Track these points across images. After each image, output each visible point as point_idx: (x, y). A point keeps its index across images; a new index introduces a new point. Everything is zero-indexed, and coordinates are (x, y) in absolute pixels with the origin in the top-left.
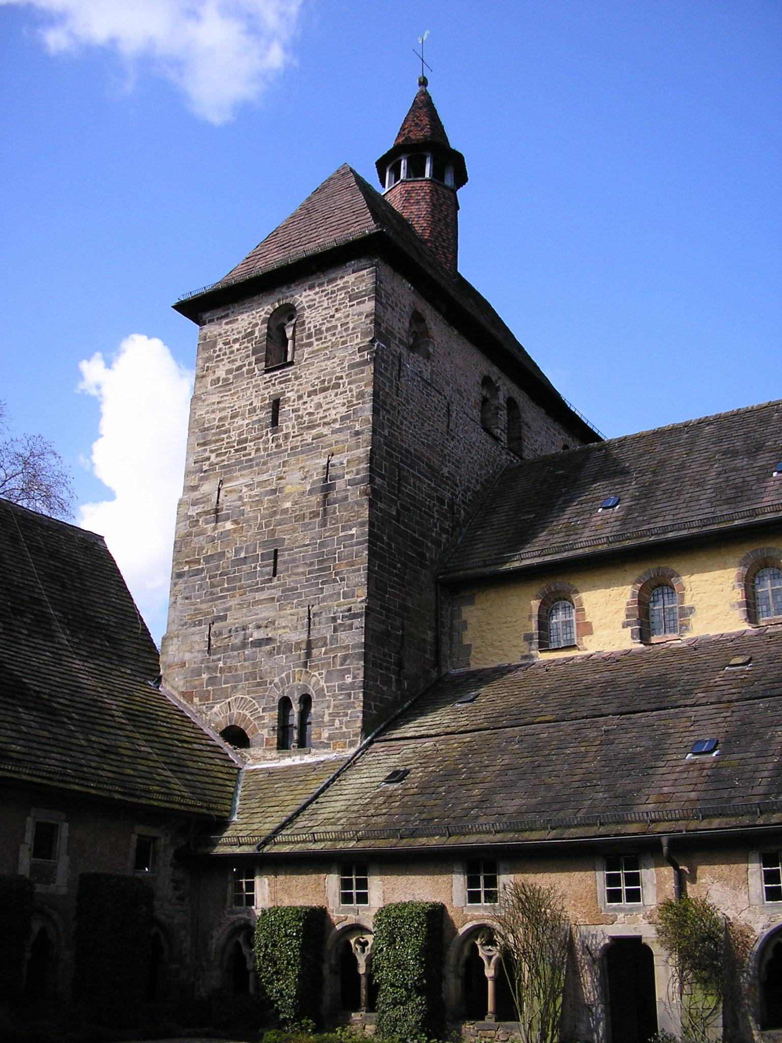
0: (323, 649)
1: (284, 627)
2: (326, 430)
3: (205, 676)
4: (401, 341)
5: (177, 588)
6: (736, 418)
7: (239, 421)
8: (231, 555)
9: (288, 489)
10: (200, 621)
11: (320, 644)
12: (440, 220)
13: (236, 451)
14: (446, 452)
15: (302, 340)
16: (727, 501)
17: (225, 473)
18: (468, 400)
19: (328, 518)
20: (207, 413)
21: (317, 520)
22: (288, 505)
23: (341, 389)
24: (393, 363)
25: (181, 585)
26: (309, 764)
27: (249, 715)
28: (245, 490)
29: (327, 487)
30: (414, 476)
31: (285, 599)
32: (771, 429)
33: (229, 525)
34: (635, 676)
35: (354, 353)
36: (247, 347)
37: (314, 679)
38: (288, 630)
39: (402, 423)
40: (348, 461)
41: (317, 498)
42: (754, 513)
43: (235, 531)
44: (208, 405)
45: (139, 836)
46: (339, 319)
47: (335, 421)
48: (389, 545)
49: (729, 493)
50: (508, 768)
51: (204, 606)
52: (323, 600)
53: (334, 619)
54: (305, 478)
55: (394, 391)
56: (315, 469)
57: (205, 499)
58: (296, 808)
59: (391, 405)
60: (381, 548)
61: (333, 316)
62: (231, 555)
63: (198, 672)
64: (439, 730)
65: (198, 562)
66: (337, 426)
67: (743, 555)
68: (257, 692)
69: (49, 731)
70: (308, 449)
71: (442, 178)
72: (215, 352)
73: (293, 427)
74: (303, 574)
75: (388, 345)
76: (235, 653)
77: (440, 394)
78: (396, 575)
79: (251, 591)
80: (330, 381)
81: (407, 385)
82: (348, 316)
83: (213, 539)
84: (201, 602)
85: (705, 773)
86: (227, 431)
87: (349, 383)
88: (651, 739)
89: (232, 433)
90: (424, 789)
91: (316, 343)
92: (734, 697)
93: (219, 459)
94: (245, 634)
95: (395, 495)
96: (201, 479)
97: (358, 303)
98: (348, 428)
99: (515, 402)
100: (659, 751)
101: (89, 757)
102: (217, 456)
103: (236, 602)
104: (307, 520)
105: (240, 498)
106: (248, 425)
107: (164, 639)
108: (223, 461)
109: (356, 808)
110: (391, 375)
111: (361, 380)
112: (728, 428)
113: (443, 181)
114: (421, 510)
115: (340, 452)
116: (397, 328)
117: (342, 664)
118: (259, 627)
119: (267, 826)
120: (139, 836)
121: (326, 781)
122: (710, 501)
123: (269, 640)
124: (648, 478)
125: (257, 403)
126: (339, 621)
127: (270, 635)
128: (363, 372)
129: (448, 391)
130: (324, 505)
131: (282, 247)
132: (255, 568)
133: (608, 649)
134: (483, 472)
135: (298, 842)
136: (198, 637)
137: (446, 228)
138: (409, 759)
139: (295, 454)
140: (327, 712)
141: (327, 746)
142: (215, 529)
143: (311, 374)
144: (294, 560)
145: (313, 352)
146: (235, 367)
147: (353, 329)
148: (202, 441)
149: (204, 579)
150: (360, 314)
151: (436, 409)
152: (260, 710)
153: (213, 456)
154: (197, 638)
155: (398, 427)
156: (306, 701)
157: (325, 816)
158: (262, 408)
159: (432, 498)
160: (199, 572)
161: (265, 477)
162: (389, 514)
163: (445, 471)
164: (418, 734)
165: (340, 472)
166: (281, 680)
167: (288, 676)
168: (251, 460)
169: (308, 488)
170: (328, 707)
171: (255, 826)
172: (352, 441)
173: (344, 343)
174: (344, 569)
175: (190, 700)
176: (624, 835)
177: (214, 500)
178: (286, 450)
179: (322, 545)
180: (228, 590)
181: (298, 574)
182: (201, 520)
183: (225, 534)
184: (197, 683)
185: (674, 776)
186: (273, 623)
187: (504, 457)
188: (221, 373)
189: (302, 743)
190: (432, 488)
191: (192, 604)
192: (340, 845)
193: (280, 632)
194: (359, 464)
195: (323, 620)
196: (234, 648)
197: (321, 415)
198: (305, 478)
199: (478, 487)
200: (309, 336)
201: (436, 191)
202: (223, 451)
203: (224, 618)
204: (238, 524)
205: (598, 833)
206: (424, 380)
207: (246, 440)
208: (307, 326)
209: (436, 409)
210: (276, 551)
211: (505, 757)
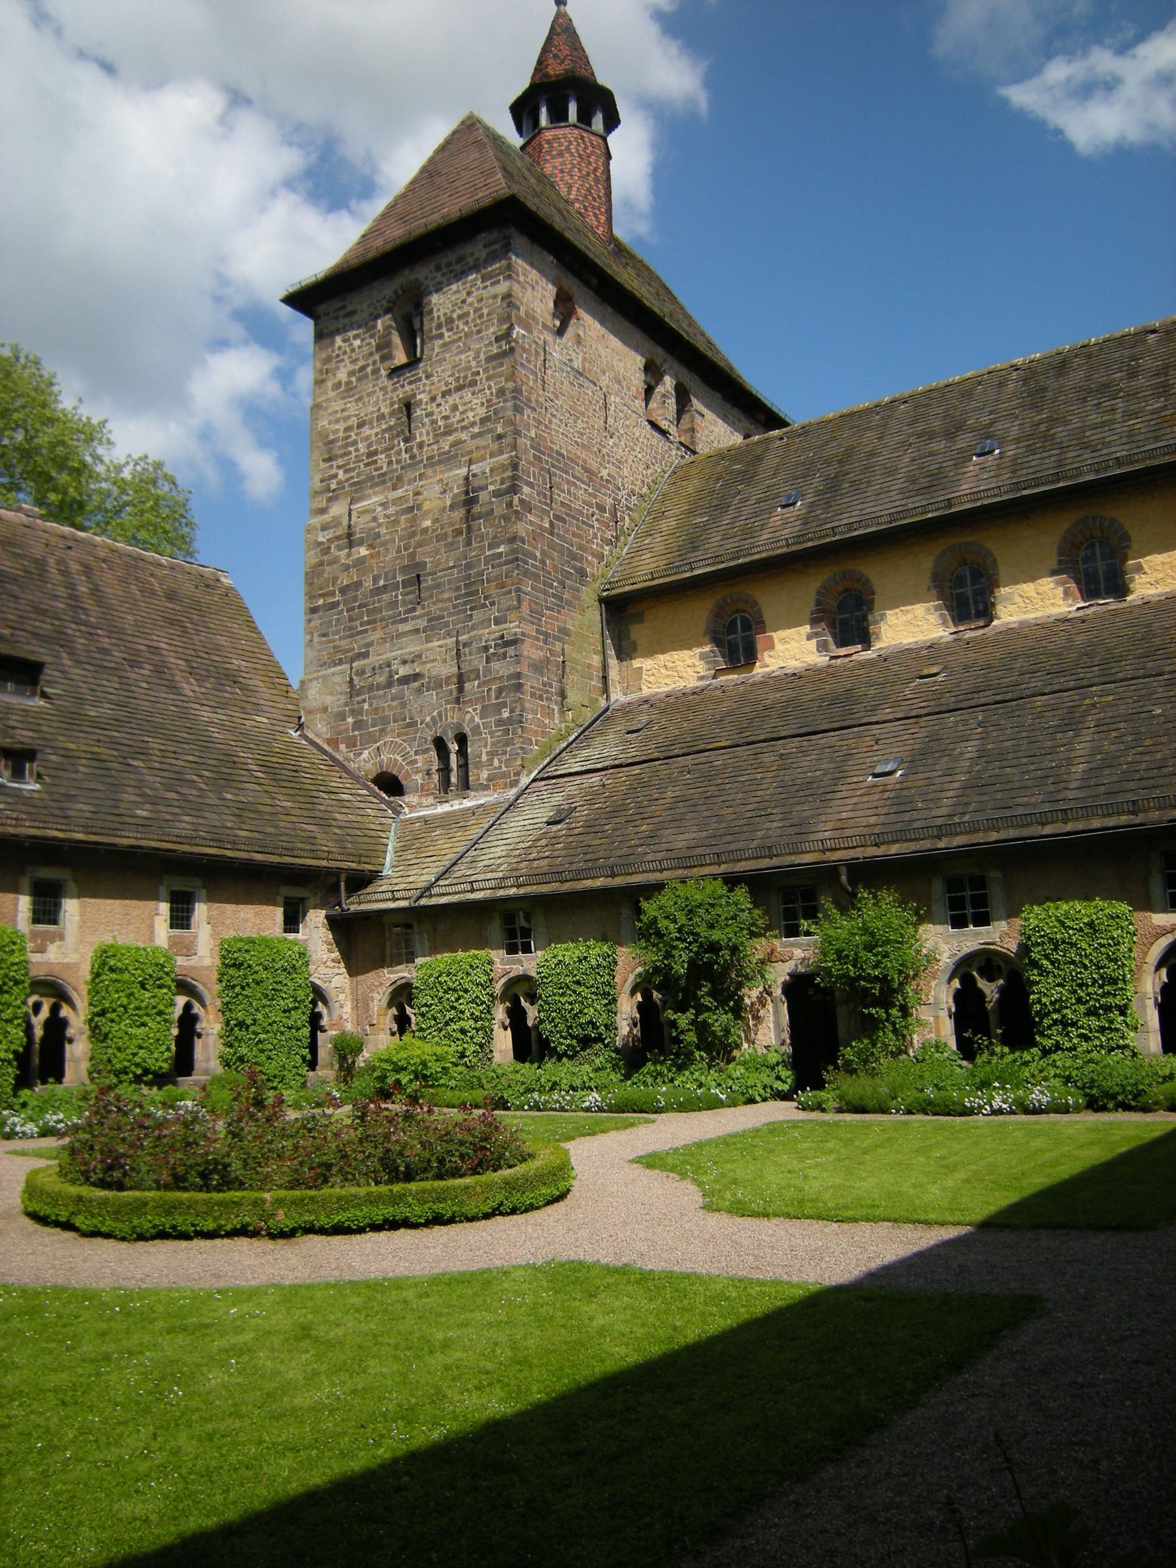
0: (476, 683)
1: (433, 661)
2: (464, 436)
3: (350, 720)
4: (545, 326)
5: (313, 624)
6: (933, 395)
7: (367, 431)
8: (368, 584)
9: (426, 506)
10: (340, 660)
11: (472, 677)
12: (588, 174)
13: (366, 465)
14: (605, 451)
15: (431, 331)
16: (918, 492)
17: (356, 491)
18: (629, 389)
19: (473, 535)
20: (330, 423)
21: (461, 539)
22: (428, 523)
23: (479, 387)
24: (537, 353)
25: (316, 622)
26: (469, 809)
27: (400, 759)
28: (379, 509)
29: (469, 500)
30: (568, 482)
31: (431, 630)
32: (973, 404)
33: (363, 551)
34: (818, 693)
35: (490, 344)
36: (369, 344)
37: (468, 716)
38: (435, 664)
39: (550, 422)
40: (492, 470)
41: (460, 513)
42: (949, 503)
43: (372, 556)
44: (330, 414)
45: (286, 898)
46: (471, 305)
47: (473, 424)
48: (543, 562)
49: (924, 482)
50: (678, 800)
51: (343, 643)
52: (473, 628)
53: (486, 648)
54: (445, 491)
55: (540, 386)
56: (455, 481)
57: (336, 523)
58: (453, 856)
59: (537, 401)
60: (533, 565)
61: (464, 302)
62: (368, 584)
63: (342, 716)
64: (606, 764)
65: (333, 594)
66: (476, 430)
67: (1065, 526)
68: (407, 734)
69: (178, 792)
70: (448, 459)
71: (588, 123)
72: (333, 351)
73: (428, 434)
74: (450, 600)
75: (530, 332)
76: (381, 692)
77: (595, 384)
78: (554, 596)
79: (393, 623)
80: (465, 377)
81: (553, 377)
82: (481, 300)
83: (347, 568)
84: (340, 639)
85: (887, 795)
86: (355, 443)
87: (488, 379)
88: (832, 761)
89: (360, 445)
90: (591, 827)
91: (447, 334)
92: (923, 711)
93: (348, 476)
94: (390, 672)
95: (547, 505)
96: (330, 500)
97: (493, 284)
98: (490, 431)
99: (685, 388)
100: (839, 775)
101: (224, 817)
102: (346, 472)
103: (378, 636)
104: (450, 539)
105: (375, 519)
106: (376, 434)
107: (302, 682)
108: (352, 478)
109: (517, 852)
110: (535, 366)
111: (500, 375)
112: (926, 406)
113: (589, 124)
114: (578, 520)
115: (483, 459)
116: (539, 311)
117: (497, 698)
118: (404, 662)
119: (424, 878)
120: (286, 898)
121: (486, 826)
122: (901, 491)
123: (416, 676)
124: (832, 470)
125: (385, 410)
126: (492, 651)
127: (417, 670)
128: (502, 365)
129: (604, 381)
130: (467, 521)
131: (402, 219)
132: (396, 596)
133: (794, 665)
134: (649, 472)
135: (456, 893)
136: (339, 675)
137: (596, 184)
138: (574, 796)
139: (432, 465)
140: (484, 750)
141: (487, 788)
142: (349, 555)
143: (443, 371)
144: (438, 586)
145: (445, 345)
146: (357, 368)
147: (489, 314)
148: (327, 456)
149: (341, 612)
150: (495, 297)
151: (590, 402)
152: (412, 753)
153: (341, 472)
154: (338, 679)
155: (546, 427)
156: (462, 739)
157: (485, 863)
158: (392, 414)
159: (590, 505)
160: (335, 605)
161: (400, 493)
162: (542, 528)
163: (604, 473)
164: (583, 769)
165: (482, 483)
166: (433, 719)
167: (440, 714)
168: (384, 475)
169: (448, 503)
170: (486, 746)
171: (411, 879)
172: (494, 446)
173: (479, 332)
174: (493, 592)
175: (336, 748)
176: (800, 865)
177: (345, 522)
178: (422, 461)
179: (469, 566)
180: (369, 623)
181: (442, 601)
182: (333, 546)
183: (361, 561)
184: (342, 728)
185: (855, 800)
186: (420, 656)
187: (674, 452)
188: (342, 375)
189: (465, 785)
190: (590, 494)
191: (329, 642)
192: (501, 893)
193: (428, 666)
194: (504, 472)
195: (474, 650)
196: (379, 688)
197: (458, 418)
198: (445, 491)
199: (645, 490)
200: (439, 326)
201: (582, 138)
202: (352, 466)
203: (366, 655)
204: (374, 548)
205: (770, 865)
206: (573, 369)
207: (375, 453)
208: (435, 315)
209: (590, 402)
210: (418, 576)
211: (677, 788)
